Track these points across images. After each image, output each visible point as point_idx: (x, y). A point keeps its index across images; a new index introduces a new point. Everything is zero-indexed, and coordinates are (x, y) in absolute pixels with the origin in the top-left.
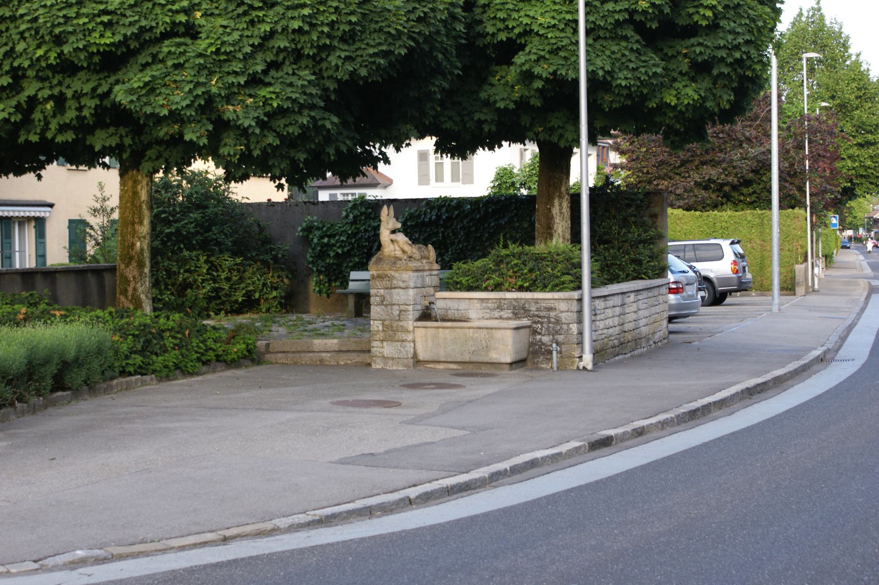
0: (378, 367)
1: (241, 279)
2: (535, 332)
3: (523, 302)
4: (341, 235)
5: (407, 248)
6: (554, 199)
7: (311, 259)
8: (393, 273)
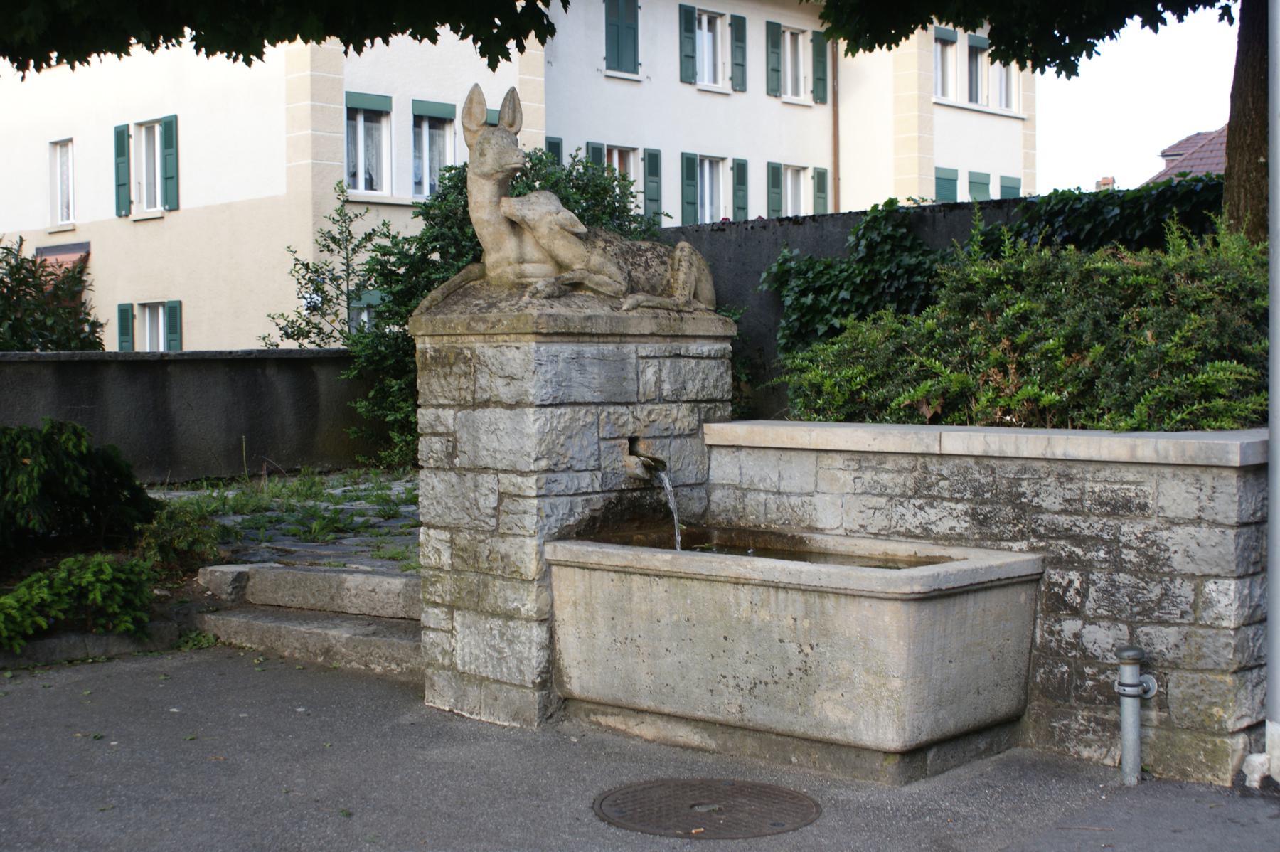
2: (1057, 605)
4: (841, 287)
8: (478, 344)
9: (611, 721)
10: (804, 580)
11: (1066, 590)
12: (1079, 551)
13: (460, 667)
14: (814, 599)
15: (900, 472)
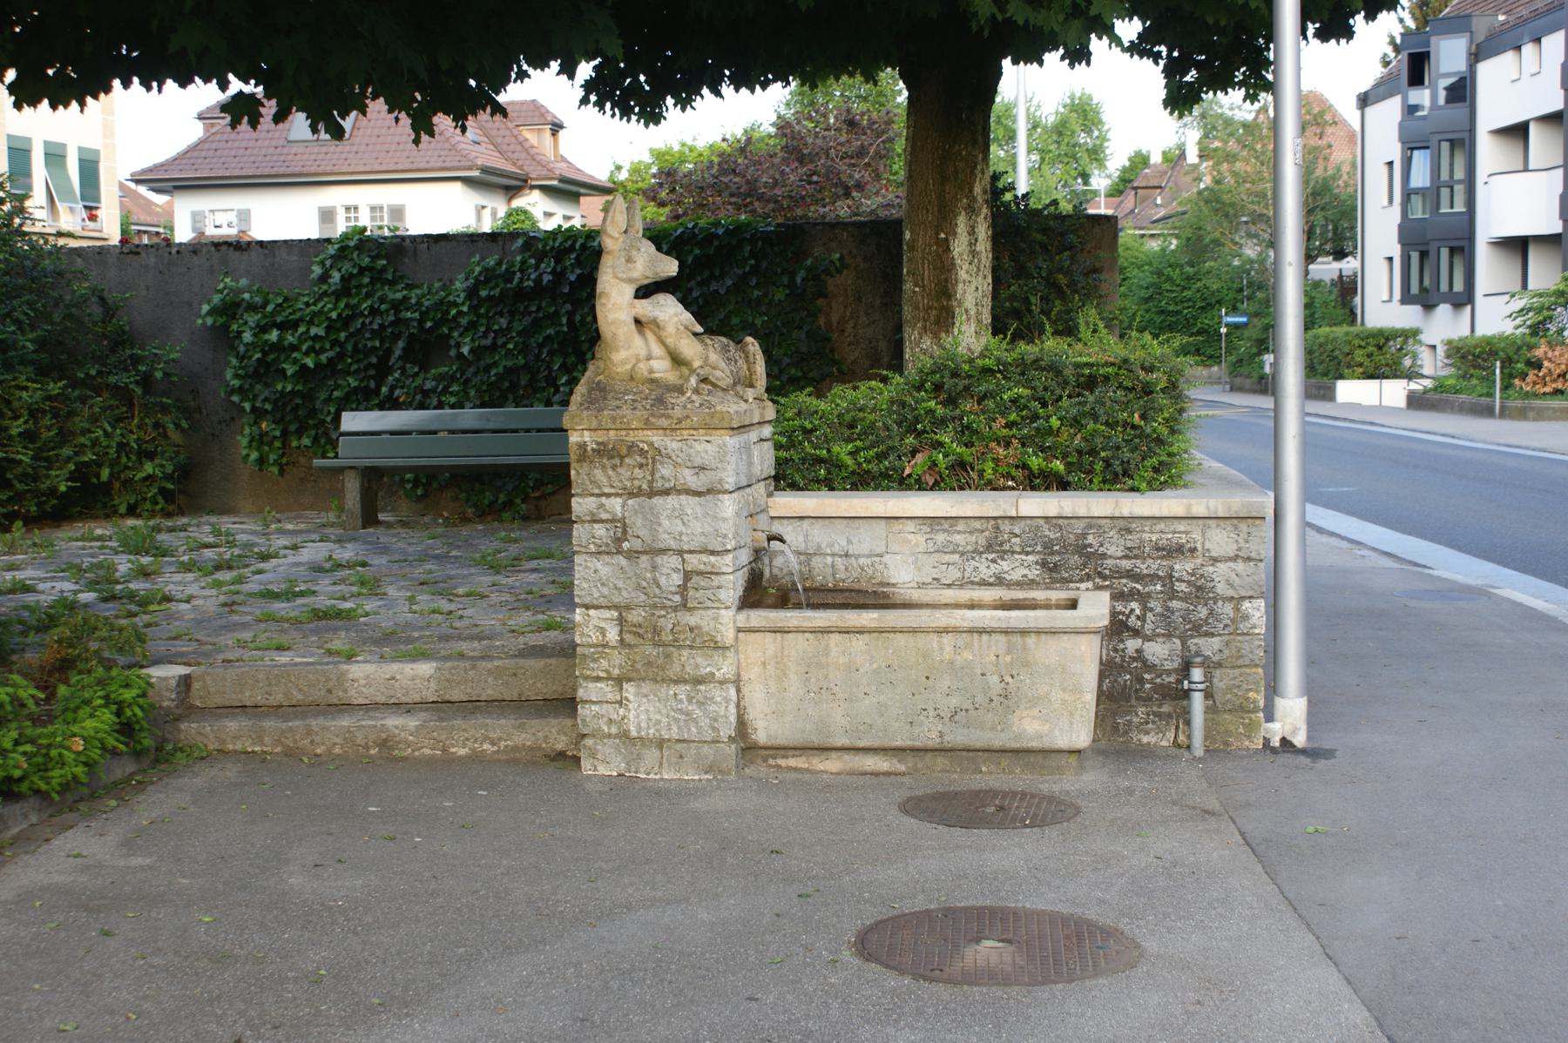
0: (603, 770)
1: (64, 436)
3: (1079, 527)
4: (311, 323)
5: (690, 348)
6: (956, 215)
7: (236, 383)
8: (657, 438)
9: (792, 762)
10: (1013, 624)
11: (1128, 617)
12: (1138, 586)
13: (634, 733)
14: (1017, 639)
15: (971, 533)
